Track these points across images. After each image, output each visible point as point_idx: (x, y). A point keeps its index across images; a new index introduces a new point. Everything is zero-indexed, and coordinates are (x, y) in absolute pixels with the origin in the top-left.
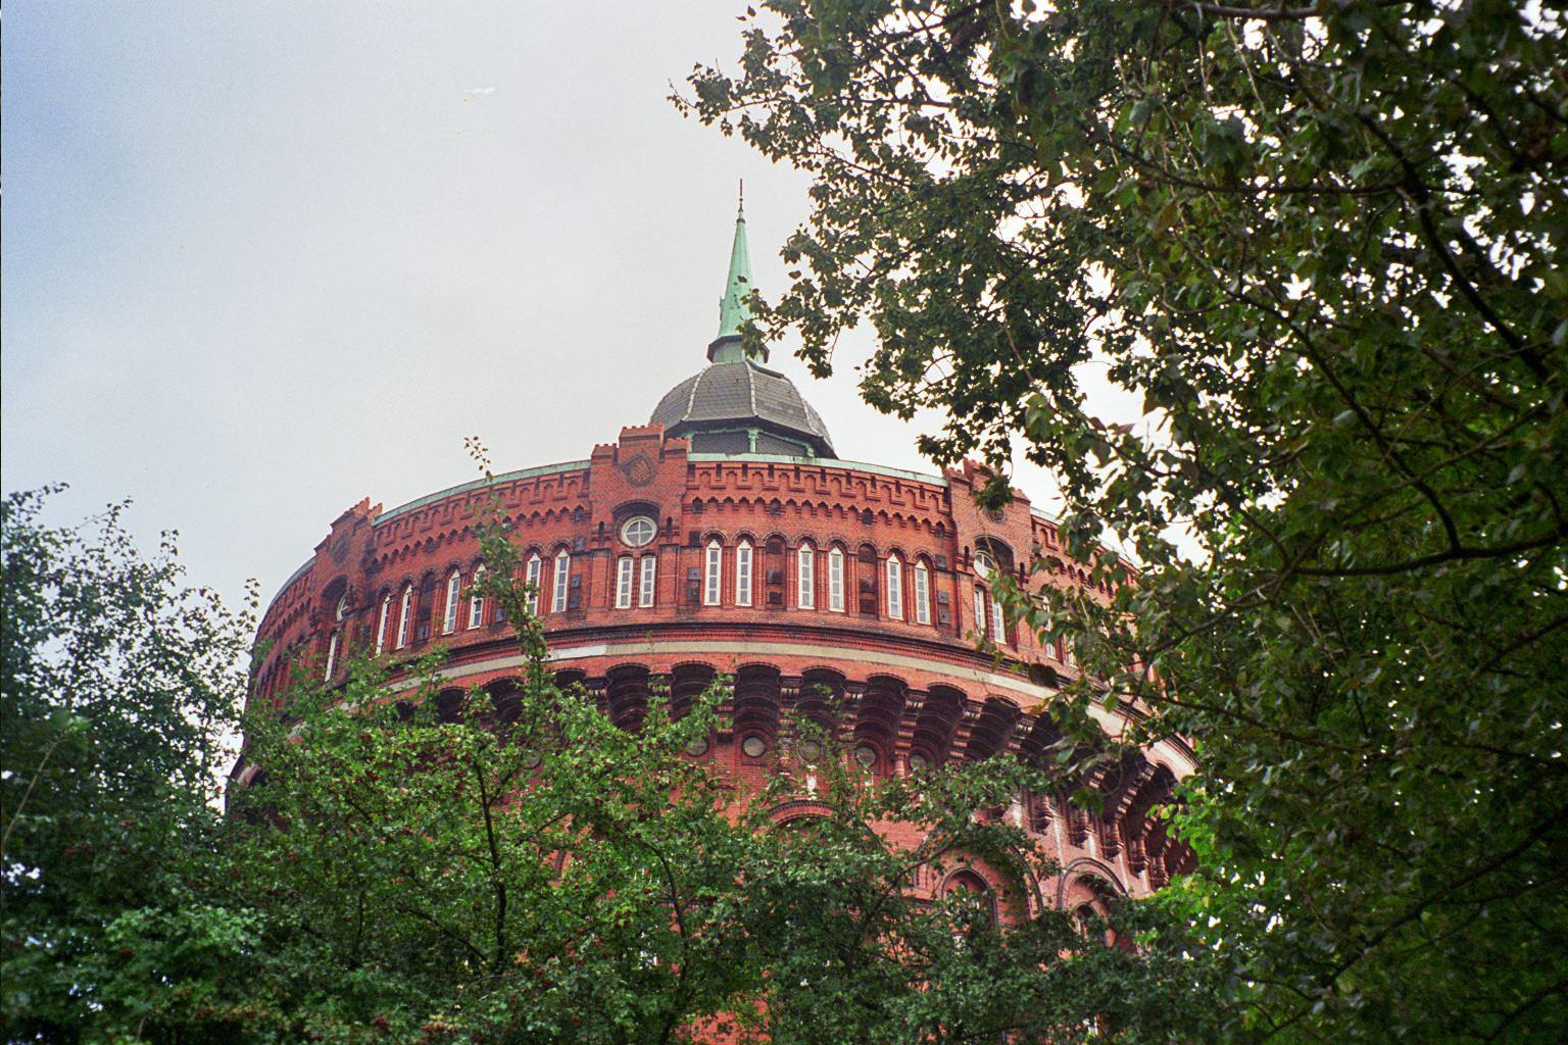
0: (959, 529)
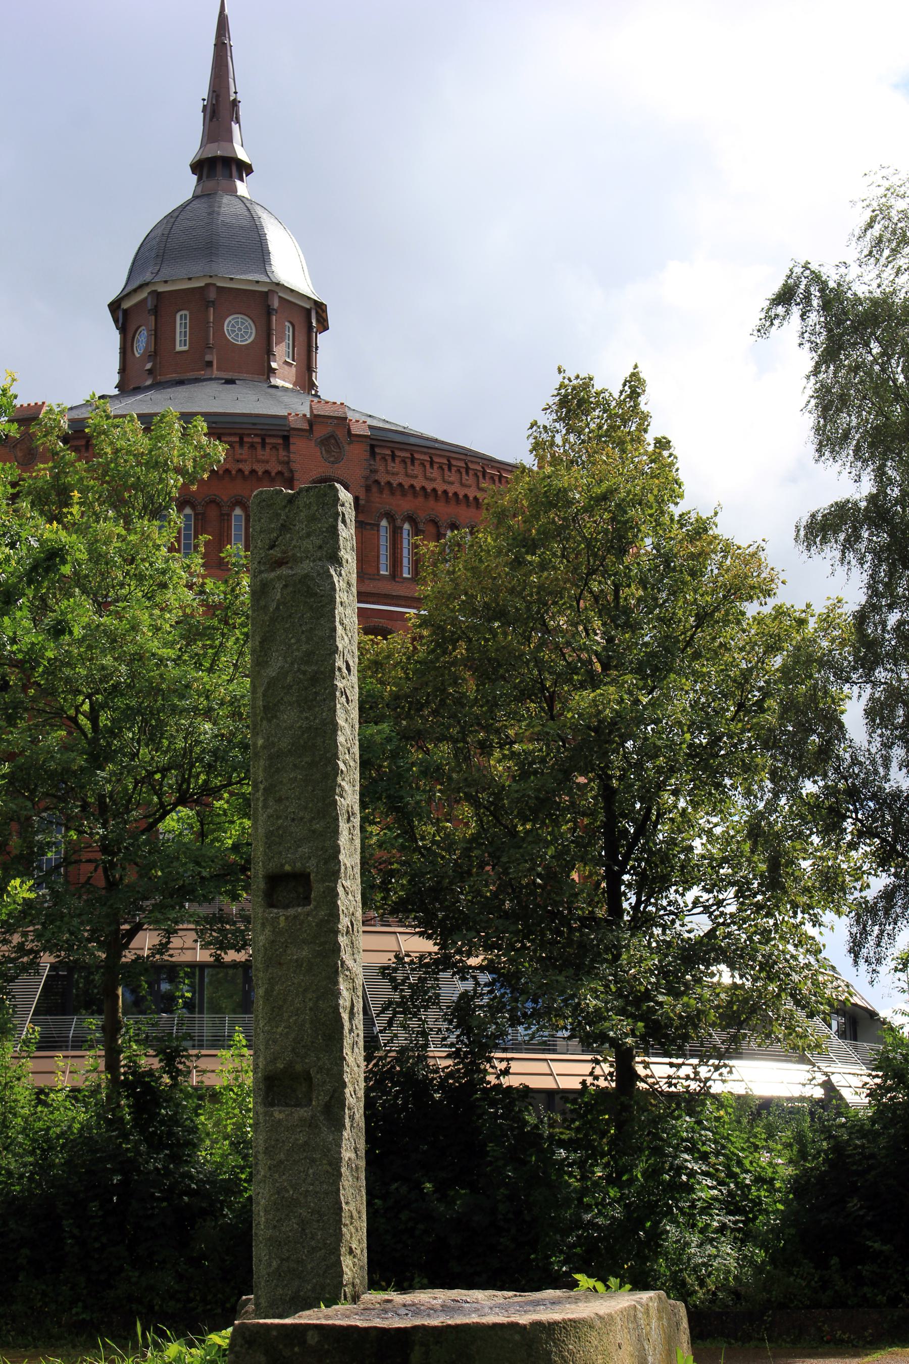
0: (297, 476)
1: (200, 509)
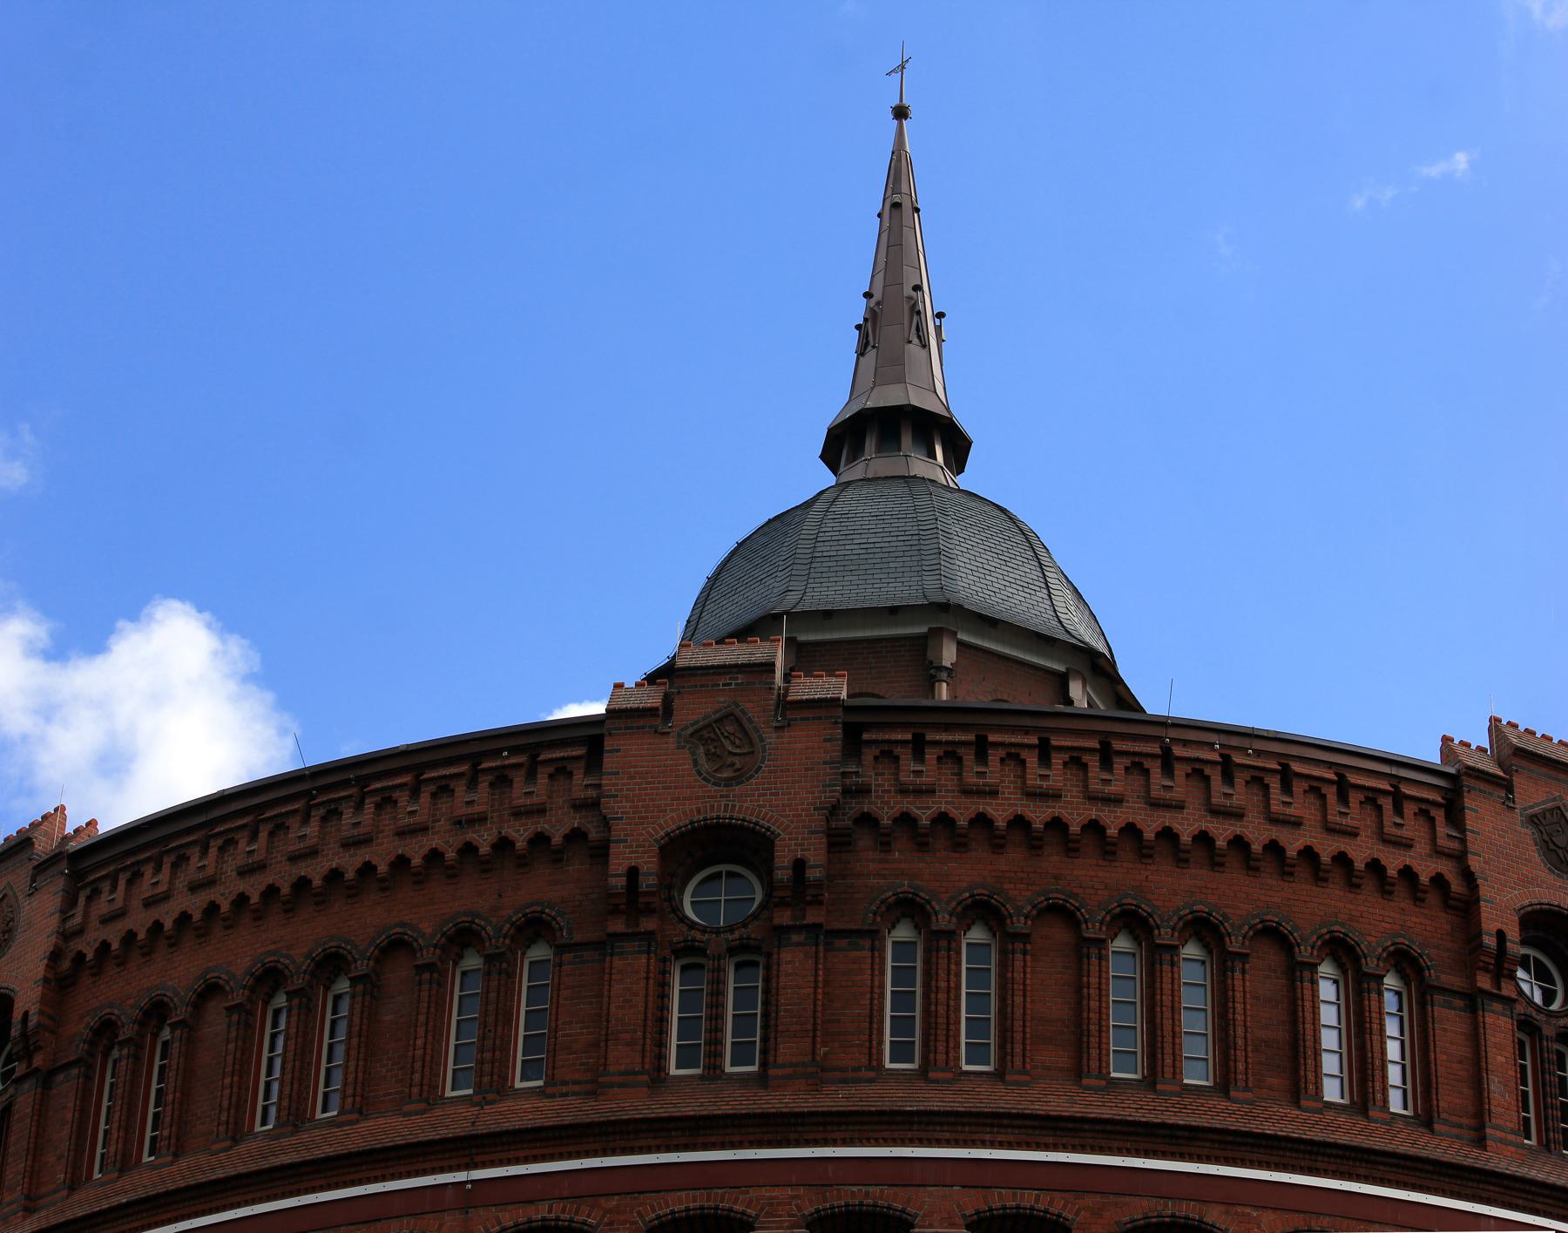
0: (1485, 891)
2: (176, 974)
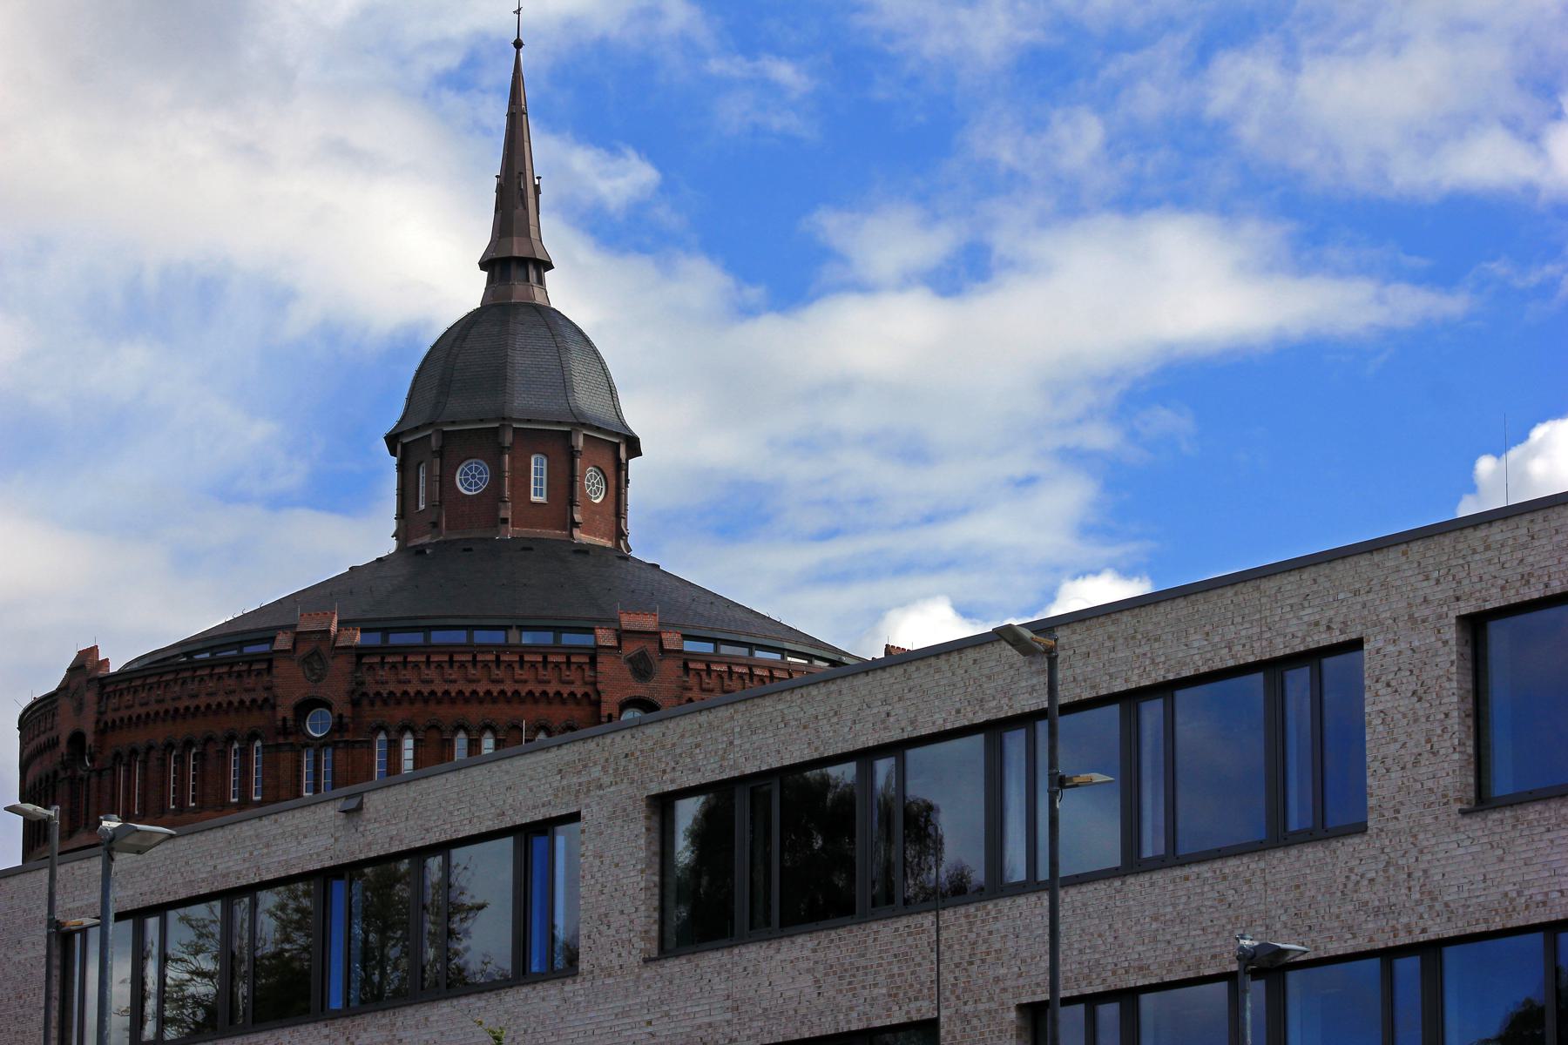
0: (604, 697)
1: (393, 735)
2: (139, 738)
